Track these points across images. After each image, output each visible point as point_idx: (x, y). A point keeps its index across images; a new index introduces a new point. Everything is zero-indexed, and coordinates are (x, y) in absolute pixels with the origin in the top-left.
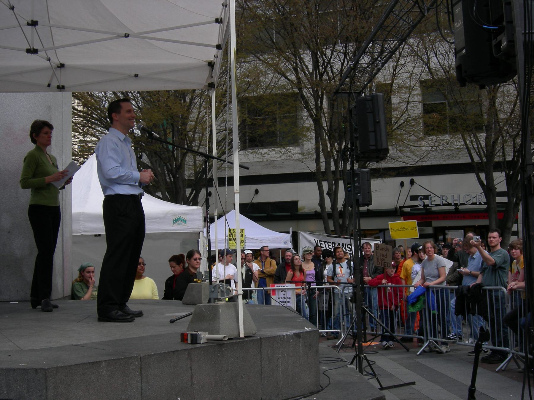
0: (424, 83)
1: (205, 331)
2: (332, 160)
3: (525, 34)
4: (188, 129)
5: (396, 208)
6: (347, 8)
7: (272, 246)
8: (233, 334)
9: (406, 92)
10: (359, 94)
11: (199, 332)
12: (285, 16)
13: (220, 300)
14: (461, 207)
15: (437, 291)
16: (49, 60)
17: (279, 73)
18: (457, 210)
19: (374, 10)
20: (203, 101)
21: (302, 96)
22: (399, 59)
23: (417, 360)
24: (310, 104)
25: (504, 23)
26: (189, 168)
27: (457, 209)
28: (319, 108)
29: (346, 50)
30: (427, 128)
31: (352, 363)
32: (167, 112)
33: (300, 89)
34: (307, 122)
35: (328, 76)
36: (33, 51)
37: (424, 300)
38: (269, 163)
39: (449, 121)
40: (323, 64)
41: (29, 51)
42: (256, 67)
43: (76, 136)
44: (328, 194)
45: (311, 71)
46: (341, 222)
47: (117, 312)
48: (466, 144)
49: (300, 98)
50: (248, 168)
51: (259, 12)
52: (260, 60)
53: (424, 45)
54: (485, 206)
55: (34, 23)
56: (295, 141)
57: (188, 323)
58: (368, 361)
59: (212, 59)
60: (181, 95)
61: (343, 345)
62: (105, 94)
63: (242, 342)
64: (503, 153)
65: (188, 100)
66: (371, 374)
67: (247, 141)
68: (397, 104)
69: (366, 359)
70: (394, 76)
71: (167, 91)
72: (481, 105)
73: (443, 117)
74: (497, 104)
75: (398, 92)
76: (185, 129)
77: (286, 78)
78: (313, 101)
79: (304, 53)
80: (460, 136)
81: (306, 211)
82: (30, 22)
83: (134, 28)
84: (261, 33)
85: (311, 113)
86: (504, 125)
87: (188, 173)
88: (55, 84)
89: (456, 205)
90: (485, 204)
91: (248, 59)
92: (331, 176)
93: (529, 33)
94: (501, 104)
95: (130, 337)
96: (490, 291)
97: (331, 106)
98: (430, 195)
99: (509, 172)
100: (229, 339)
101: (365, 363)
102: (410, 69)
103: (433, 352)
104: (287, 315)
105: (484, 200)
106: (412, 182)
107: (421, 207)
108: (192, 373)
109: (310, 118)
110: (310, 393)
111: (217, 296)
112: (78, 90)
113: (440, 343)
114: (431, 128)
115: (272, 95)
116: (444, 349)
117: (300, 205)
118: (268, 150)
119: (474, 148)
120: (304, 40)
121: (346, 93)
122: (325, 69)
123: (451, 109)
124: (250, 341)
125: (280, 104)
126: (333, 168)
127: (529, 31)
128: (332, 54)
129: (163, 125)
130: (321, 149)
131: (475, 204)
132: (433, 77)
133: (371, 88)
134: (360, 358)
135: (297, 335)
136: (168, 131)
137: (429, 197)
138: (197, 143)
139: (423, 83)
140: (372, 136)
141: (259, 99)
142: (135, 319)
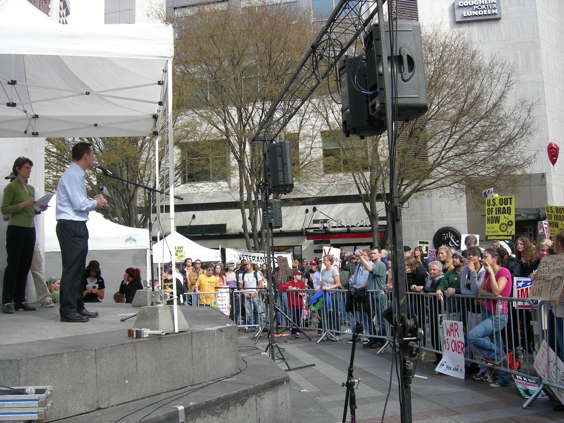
0: (308, 138)
1: (147, 327)
2: (252, 192)
3: (392, 98)
4: (139, 167)
5: (302, 230)
6: (265, 75)
7: (204, 259)
8: (170, 330)
9: (309, 140)
10: (272, 141)
11: (143, 329)
12: (216, 80)
13: (159, 303)
14: (352, 229)
15: (332, 294)
16: (26, 112)
17: (212, 124)
18: (349, 232)
19: (286, 77)
20: (151, 146)
21: (230, 142)
22: (304, 115)
23: (317, 347)
24: (236, 149)
25: (378, 90)
26: (140, 198)
27: (348, 230)
28: (243, 151)
29: (263, 107)
30: (326, 168)
31: (266, 351)
32: (123, 153)
33: (228, 137)
34: (233, 162)
35: (250, 127)
36: (12, 105)
37: (323, 301)
38: (203, 194)
39: (343, 163)
40: (246, 117)
41: (8, 105)
42: (193, 119)
43: (50, 172)
44: (250, 219)
45: (236, 122)
46: (259, 240)
47: (75, 314)
48: (355, 180)
49: (228, 144)
50: (182, 199)
51: (197, 76)
52: (196, 113)
53: (323, 103)
54: (370, 228)
55: (13, 83)
56: (225, 177)
57: (134, 322)
58: (278, 348)
59: (156, 112)
60: (134, 141)
61: (260, 336)
62: (74, 139)
63: (176, 336)
64: (383, 187)
65: (140, 145)
66: (281, 359)
67: (187, 177)
68: (302, 149)
69: (276, 346)
70: (301, 127)
71: (122, 137)
72: (366, 151)
73: (337, 160)
74: (378, 150)
75: (303, 140)
76: (137, 168)
77: (217, 128)
78: (238, 146)
79: (231, 109)
80: (351, 174)
81: (233, 232)
82: (10, 82)
83: (93, 87)
84: (198, 93)
85: (236, 155)
86: (384, 166)
87: (140, 201)
88: (30, 131)
89: (348, 227)
90: (370, 226)
91: (188, 113)
92: (252, 205)
93: (395, 98)
94: (382, 150)
95: (88, 333)
96: (372, 293)
97: (253, 150)
98: (328, 220)
99: (388, 202)
100: (166, 334)
101: (276, 350)
102: (313, 122)
103: (328, 340)
104: (214, 314)
105: (369, 223)
106: (315, 210)
107: (322, 229)
108: (136, 361)
109: (235, 160)
110: (231, 375)
111: (157, 300)
112: (50, 136)
113: (334, 334)
114: (328, 168)
115: (206, 141)
116: (337, 338)
117: (228, 227)
118: (203, 184)
119: (361, 183)
120: (231, 99)
121: (261, 140)
122: (248, 121)
123: (344, 153)
124: (184, 335)
125: (212, 148)
126: (253, 199)
127: (395, 96)
128: (253, 109)
129: (119, 164)
130: (244, 183)
131: (362, 226)
132: (330, 129)
133: (280, 136)
134: (272, 346)
135: (221, 330)
136: (123, 169)
137: (328, 221)
138: (147, 178)
139: (323, 133)
140: (281, 174)
141: (196, 144)
142: (89, 320)
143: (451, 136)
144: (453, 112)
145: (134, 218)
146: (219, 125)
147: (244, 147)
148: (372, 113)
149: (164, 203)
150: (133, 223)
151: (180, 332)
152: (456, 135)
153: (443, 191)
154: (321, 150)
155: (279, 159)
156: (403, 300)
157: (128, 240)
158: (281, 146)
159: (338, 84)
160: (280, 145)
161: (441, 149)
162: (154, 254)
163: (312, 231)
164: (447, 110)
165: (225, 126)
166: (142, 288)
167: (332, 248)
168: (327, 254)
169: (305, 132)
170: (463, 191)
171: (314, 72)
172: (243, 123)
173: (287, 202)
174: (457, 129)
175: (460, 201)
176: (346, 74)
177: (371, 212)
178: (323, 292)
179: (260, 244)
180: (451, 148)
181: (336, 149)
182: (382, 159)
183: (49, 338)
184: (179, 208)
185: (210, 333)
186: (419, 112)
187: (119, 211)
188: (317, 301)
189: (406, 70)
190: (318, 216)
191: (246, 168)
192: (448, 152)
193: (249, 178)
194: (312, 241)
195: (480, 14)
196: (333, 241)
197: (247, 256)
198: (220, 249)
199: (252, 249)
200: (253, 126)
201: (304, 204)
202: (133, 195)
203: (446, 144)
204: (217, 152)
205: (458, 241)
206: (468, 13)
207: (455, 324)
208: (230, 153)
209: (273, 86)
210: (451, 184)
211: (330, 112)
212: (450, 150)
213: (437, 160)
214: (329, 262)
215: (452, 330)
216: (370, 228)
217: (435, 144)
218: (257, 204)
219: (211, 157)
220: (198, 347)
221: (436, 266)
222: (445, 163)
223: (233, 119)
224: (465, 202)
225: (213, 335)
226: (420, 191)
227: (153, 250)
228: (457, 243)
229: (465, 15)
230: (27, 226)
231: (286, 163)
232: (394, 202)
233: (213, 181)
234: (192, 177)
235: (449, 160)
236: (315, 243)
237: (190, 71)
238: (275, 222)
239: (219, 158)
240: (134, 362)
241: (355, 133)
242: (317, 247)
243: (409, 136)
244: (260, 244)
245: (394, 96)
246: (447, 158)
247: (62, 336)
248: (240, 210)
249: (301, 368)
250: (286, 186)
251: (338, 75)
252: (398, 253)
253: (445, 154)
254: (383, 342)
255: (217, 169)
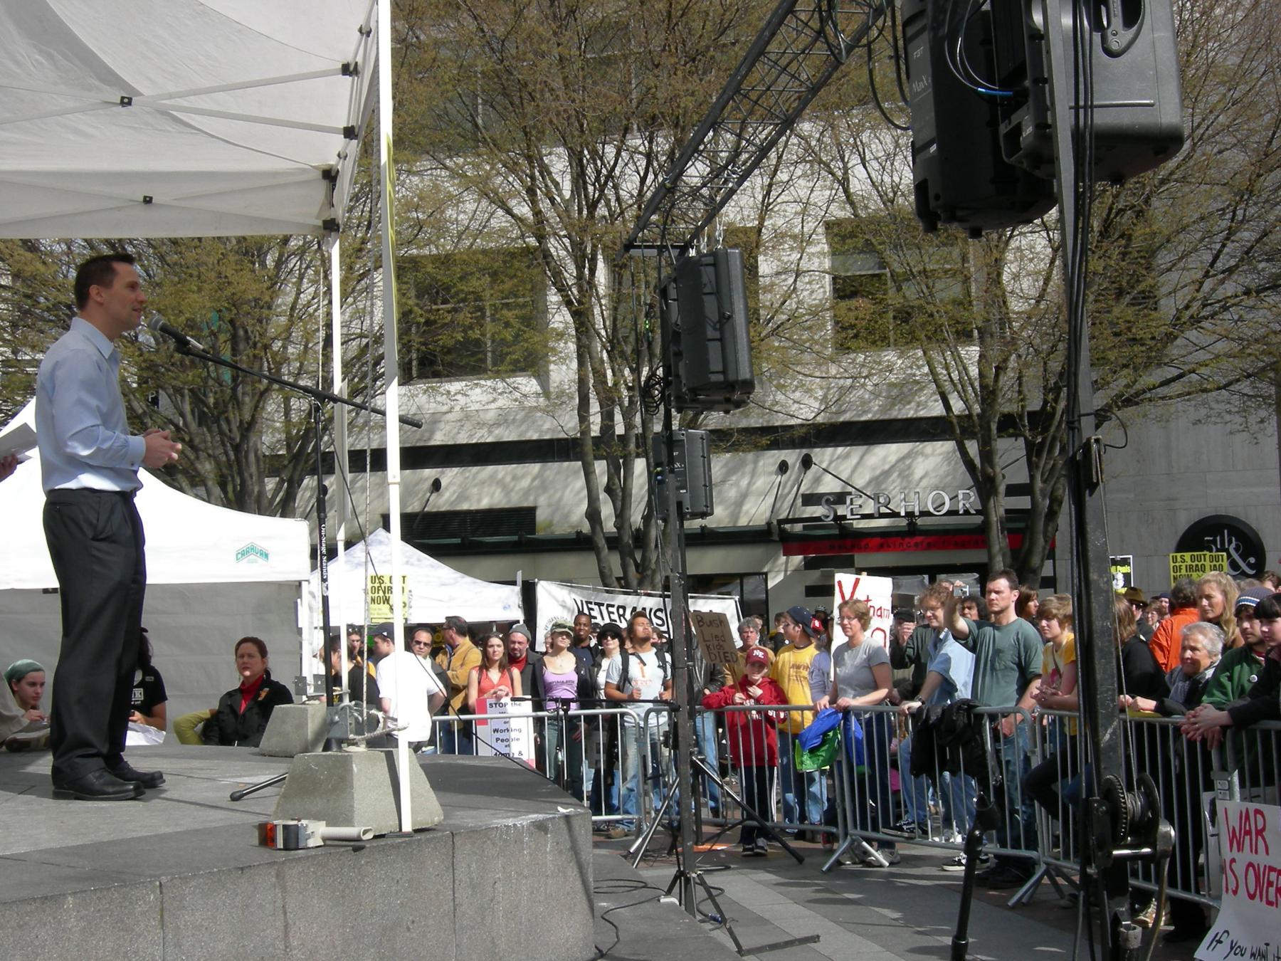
1: (317, 817)
3: (1076, 108)
5: (769, 524)
8: (388, 825)
9: (792, 249)
11: (304, 822)
21: (547, 255)
25: (1027, 83)
27: (912, 524)
28: (587, 284)
33: (541, 238)
35: (610, 210)
40: (597, 179)
44: (609, 490)
46: (638, 556)
52: (446, 168)
53: (835, 137)
54: (979, 519)
56: (533, 364)
58: (708, 889)
60: (250, 250)
61: (646, 850)
64: (1020, 392)
66: (715, 919)
67: (414, 363)
70: (765, 209)
72: (967, 280)
74: (1005, 277)
77: (509, 211)
78: (572, 269)
79: (550, 154)
80: (920, 353)
81: (561, 530)
85: (568, 296)
86: (1022, 328)
87: (270, 439)
89: (910, 515)
90: (978, 512)
91: (418, 166)
93: (1085, 107)
94: (1016, 277)
95: (135, 835)
98: (850, 493)
100: (375, 837)
101: (700, 892)
102: (803, 193)
106: (807, 463)
107: (829, 521)
109: (565, 310)
114: (851, 333)
115: (475, 253)
117: (541, 516)
118: (464, 383)
119: (952, 380)
122: (602, 191)
123: (899, 289)
126: (620, 429)
128: (618, 155)
132: (856, 215)
134: (688, 880)
135: (541, 827)
140: (714, 350)
141: (445, 261)
143: (1231, 232)
144: (1237, 159)
145: (256, 489)
146: (512, 203)
147: (593, 271)
148: (1009, 156)
149: (366, 443)
150: (251, 501)
151: (416, 831)
152: (1247, 230)
153: (1204, 403)
154: (828, 278)
155: (710, 305)
156: (1110, 731)
157: (243, 553)
158: (714, 265)
159: (898, 68)
160: (710, 260)
161: (1199, 275)
162: (330, 594)
163: (798, 527)
164: (1220, 152)
165: (534, 202)
166: (290, 701)
167: (864, 577)
168: (847, 597)
169: (780, 222)
170: (1270, 405)
171: (820, 33)
172: (586, 196)
173: (721, 439)
174: (1252, 210)
175: (1259, 436)
176: (925, 38)
177: (983, 471)
178: (841, 715)
179: (642, 568)
180: (1230, 271)
181: (873, 276)
182: (1016, 305)
183: (15, 850)
184: (414, 457)
185: (507, 834)
186: (1156, 153)
187: (207, 467)
188: (823, 743)
189: (1117, 21)
190: (817, 480)
191: (599, 334)
192: (1222, 282)
193: (607, 366)
194: (797, 560)
196: (860, 559)
197: (600, 605)
198: (519, 582)
199: (616, 583)
200: (620, 204)
201: (775, 445)
202: (253, 417)
203: (1216, 258)
204: (508, 285)
205: (1252, 560)
207: (1257, 812)
208: (544, 288)
209: (677, 82)
210: (1230, 384)
211: (854, 160)
212: (1229, 275)
213: (1187, 307)
214: (855, 622)
215: (1248, 833)
216: (979, 519)
217: (1181, 259)
218: (632, 446)
219: (490, 299)
220: (471, 879)
221: (1200, 637)
222: (1212, 316)
223: (556, 184)
224: (1275, 439)
225: (518, 841)
226: (1137, 404)
227: (330, 582)
228: (1249, 565)
231: (730, 317)
232: (1079, 430)
233: (498, 375)
234: (432, 363)
235: (1225, 309)
236: (809, 565)
237: (422, 37)
238: (691, 497)
239: (518, 306)
240: (280, 924)
241: (952, 218)
242: (814, 577)
243: (1101, 234)
244: (642, 568)
245: (1082, 103)
246: (1219, 301)
247: (54, 845)
248: (580, 463)
249: (774, 947)
250: (731, 386)
251: (901, 43)
252: (1093, 587)
253: (1214, 290)
254: (1027, 867)
255: (510, 338)
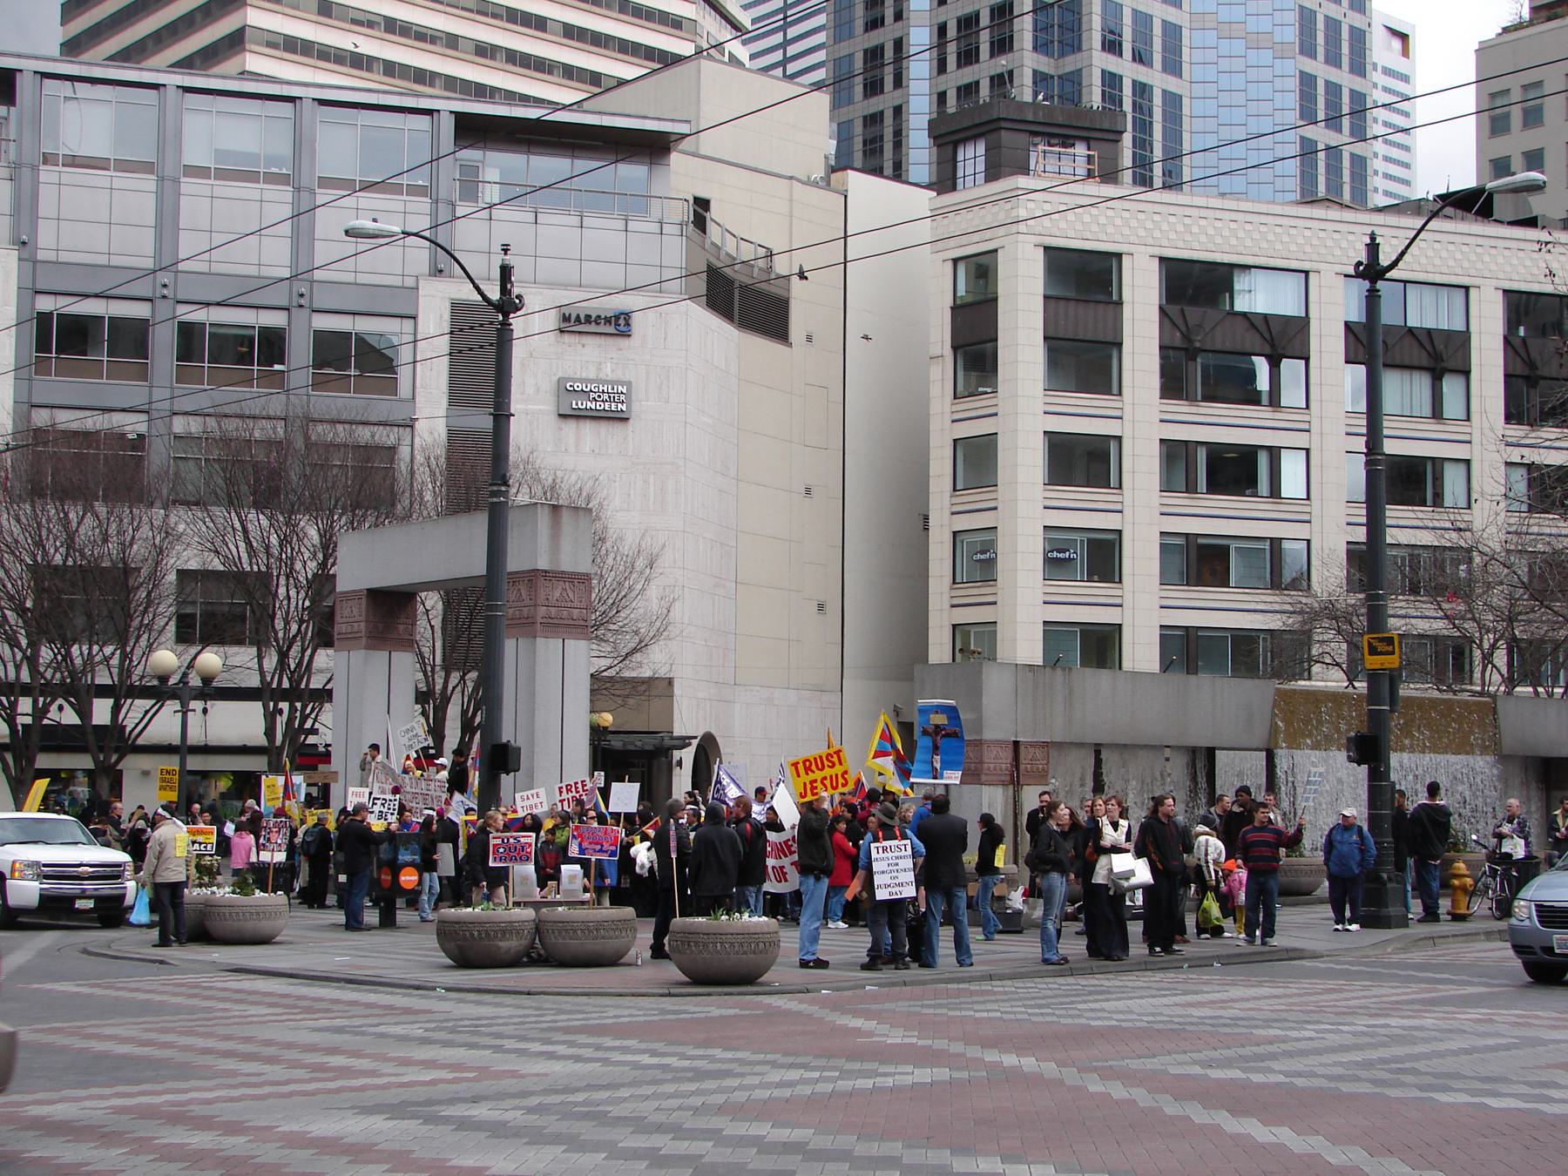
55: (866, 337)
195: (598, 408)
206: (580, 403)
229: (574, 406)
230: (26, 806)
